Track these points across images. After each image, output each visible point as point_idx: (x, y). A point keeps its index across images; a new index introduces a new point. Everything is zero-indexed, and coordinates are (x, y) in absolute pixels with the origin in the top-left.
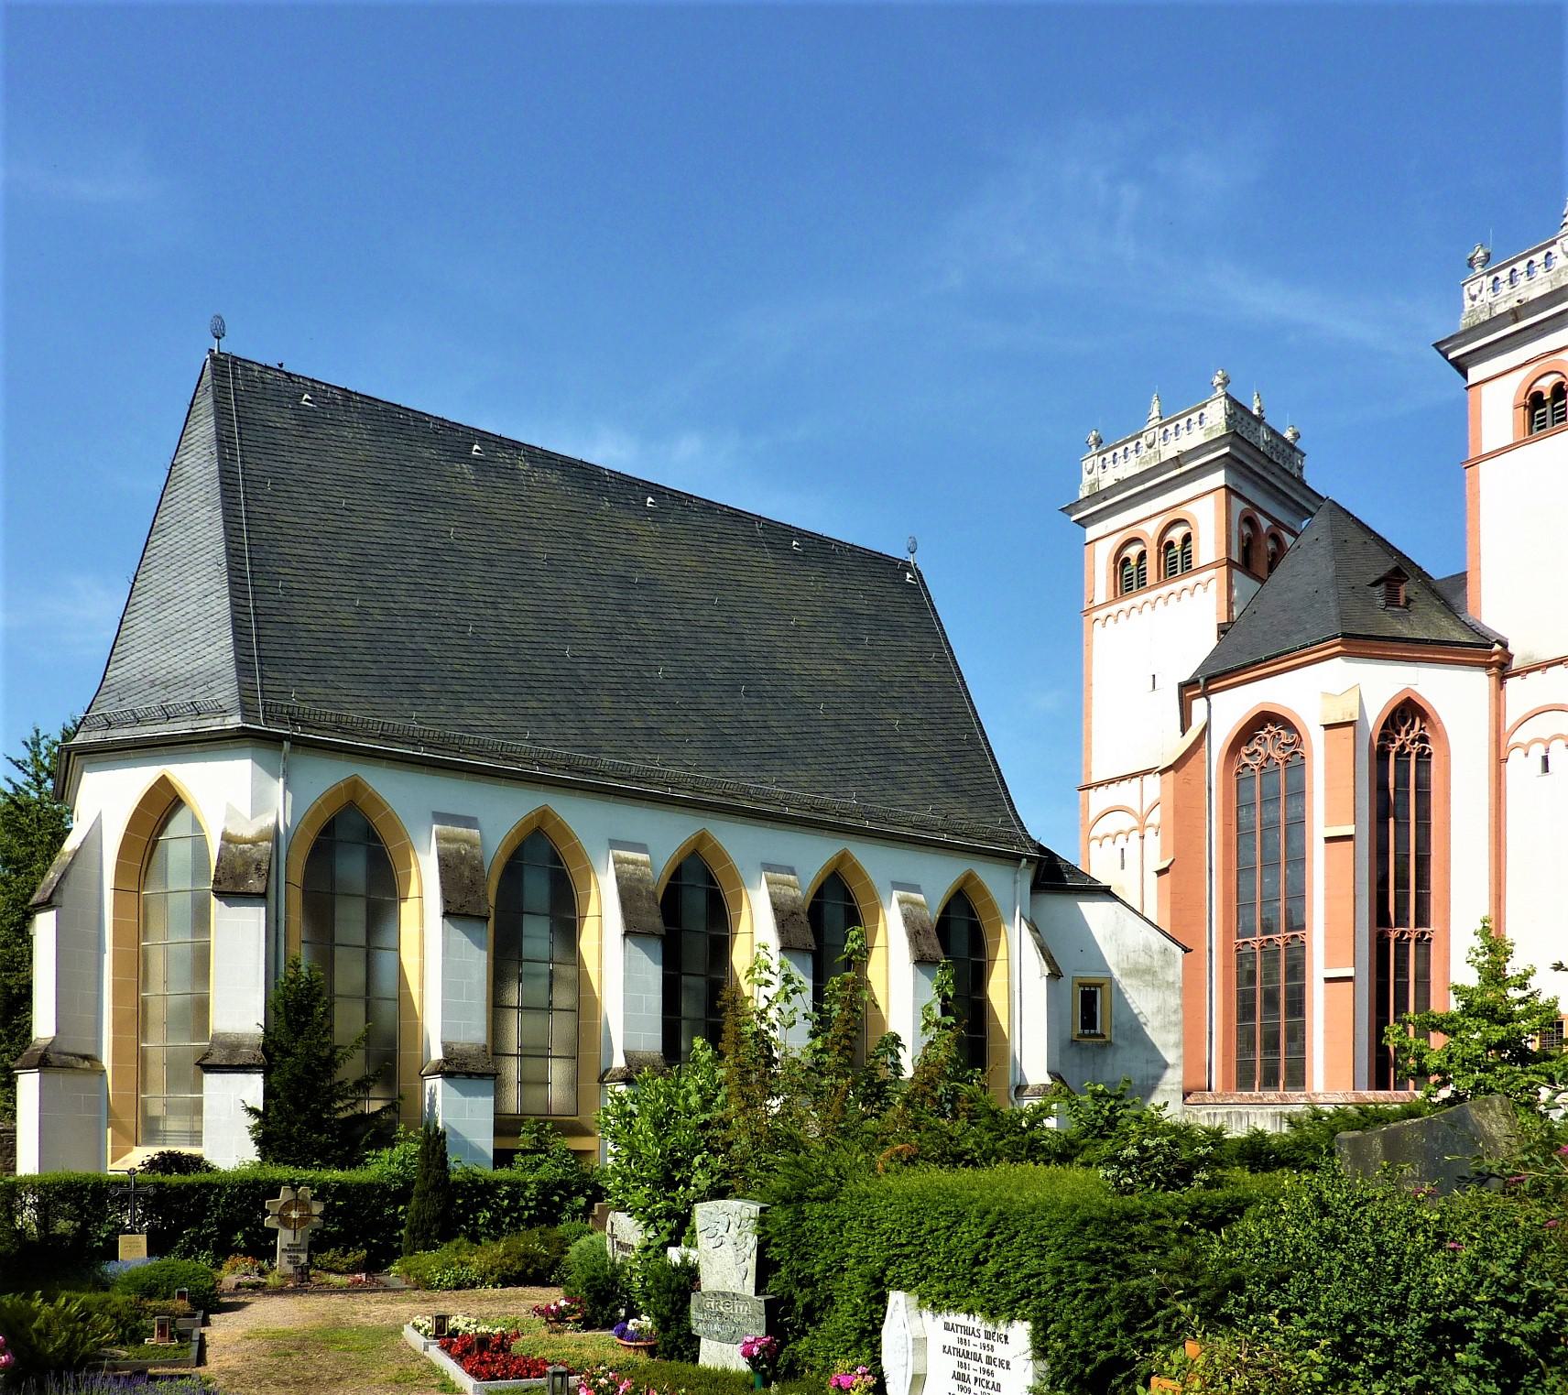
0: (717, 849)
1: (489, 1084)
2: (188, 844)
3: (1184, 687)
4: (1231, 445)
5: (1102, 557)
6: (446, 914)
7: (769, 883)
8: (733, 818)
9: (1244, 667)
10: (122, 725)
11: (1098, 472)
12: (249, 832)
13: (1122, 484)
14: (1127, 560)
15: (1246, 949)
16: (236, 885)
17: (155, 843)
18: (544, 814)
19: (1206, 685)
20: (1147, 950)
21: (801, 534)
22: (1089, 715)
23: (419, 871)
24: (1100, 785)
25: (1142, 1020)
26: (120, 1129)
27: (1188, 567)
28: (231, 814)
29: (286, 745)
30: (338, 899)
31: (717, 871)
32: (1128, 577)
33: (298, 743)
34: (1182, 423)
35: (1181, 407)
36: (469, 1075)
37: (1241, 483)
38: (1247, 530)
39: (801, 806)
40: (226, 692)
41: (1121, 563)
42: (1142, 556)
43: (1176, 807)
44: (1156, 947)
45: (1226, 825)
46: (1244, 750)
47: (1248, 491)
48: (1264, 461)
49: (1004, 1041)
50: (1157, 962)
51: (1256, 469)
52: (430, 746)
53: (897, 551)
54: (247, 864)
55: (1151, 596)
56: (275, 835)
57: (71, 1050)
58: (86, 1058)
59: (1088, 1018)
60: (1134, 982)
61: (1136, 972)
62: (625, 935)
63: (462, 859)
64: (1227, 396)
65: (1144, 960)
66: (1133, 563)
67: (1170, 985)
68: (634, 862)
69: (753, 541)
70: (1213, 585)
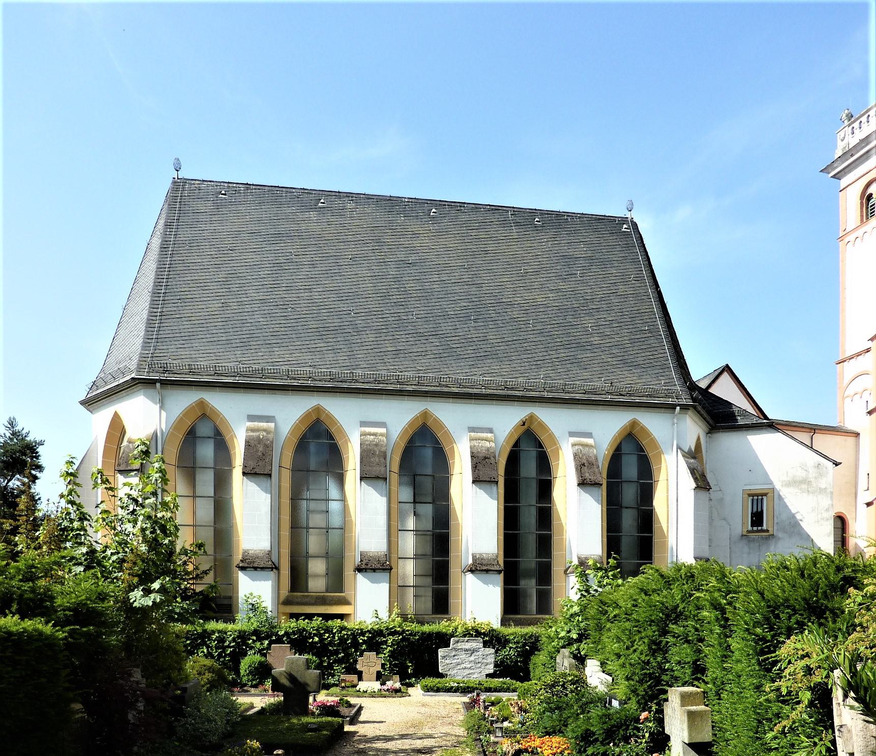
0: (437, 421)
1: (386, 575)
7: (471, 440)
8: (448, 400)
16: (127, 466)
18: (634, 424)
21: (542, 213)
24: (851, 358)
25: (798, 517)
29: (158, 385)
30: (198, 470)
31: (644, 443)
33: (165, 383)
36: (255, 568)
49: (664, 537)
50: (812, 473)
53: (618, 211)
59: (757, 519)
60: (792, 490)
61: (794, 483)
63: (259, 440)
65: (800, 474)
67: (822, 491)
68: (375, 434)
69: (504, 223)
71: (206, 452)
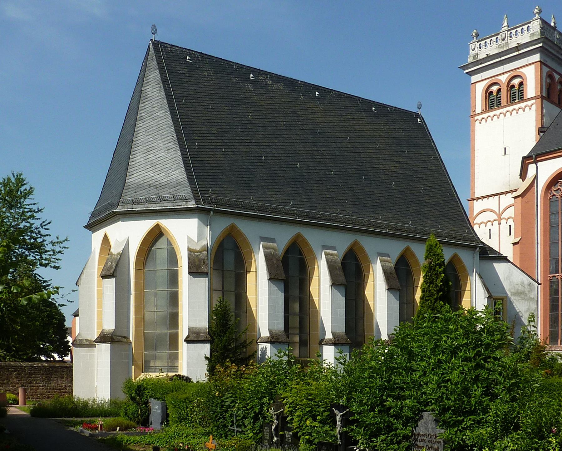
2: (165, 252)
3: (524, 159)
4: (543, 42)
5: (480, 89)
6: (271, 279)
8: (378, 236)
9: (554, 151)
10: (139, 203)
11: (477, 50)
12: (198, 248)
13: (489, 57)
14: (491, 93)
15: (554, 279)
17: (150, 250)
19: (536, 158)
20: (522, 284)
22: (473, 165)
23: (255, 261)
26: (137, 367)
27: (522, 98)
28: (190, 240)
32: (493, 101)
34: (519, 29)
35: (519, 21)
37: (547, 59)
38: (549, 81)
39: (392, 228)
40: (186, 191)
41: (488, 93)
42: (499, 91)
43: (522, 214)
44: (526, 283)
45: (545, 222)
46: (553, 188)
47: (550, 63)
50: (527, 289)
51: (553, 52)
52: (260, 211)
53: (413, 109)
54: (200, 260)
55: (504, 110)
56: (206, 248)
57: (120, 335)
58: (124, 337)
61: (518, 293)
62: (332, 285)
64: (541, 19)
65: (521, 288)
68: (332, 255)
70: (534, 106)
71: (229, 259)
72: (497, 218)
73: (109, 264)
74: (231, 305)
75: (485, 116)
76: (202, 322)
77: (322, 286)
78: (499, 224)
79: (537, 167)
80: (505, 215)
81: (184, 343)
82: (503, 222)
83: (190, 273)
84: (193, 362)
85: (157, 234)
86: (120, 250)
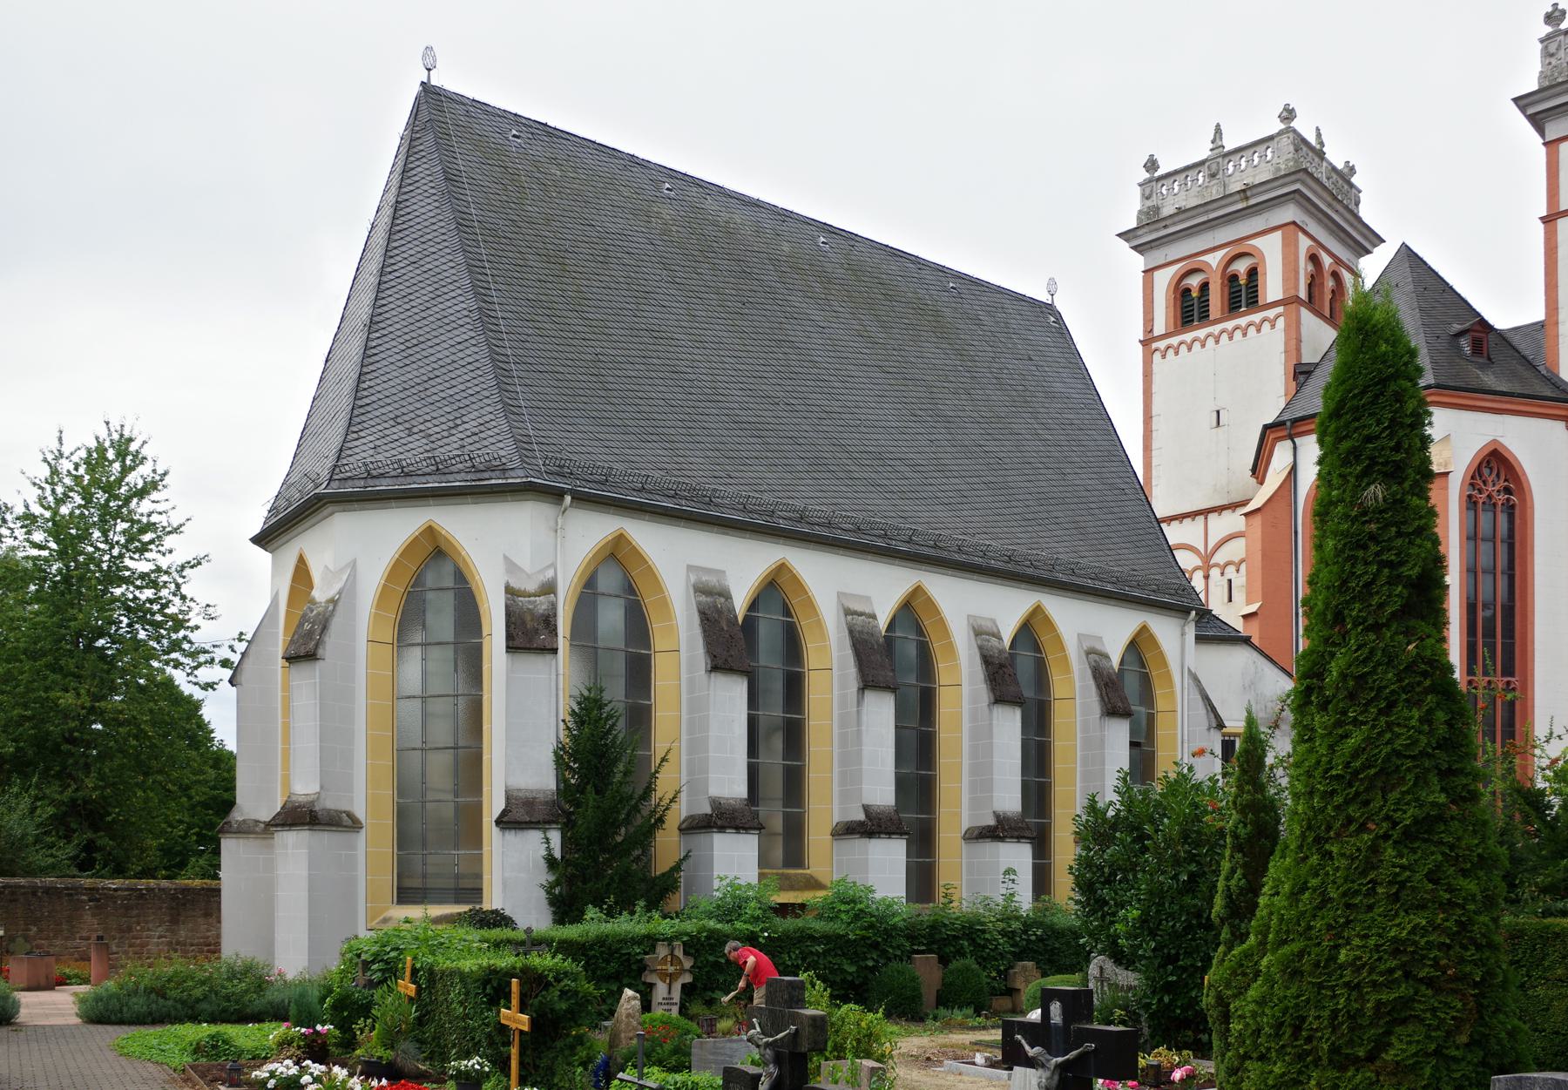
3: (1266, 428)
18: (782, 568)
29: (568, 499)
38: (1310, 267)
42: (1204, 287)
48: (1329, 199)
53: (1043, 297)
66: (1195, 294)
72: (1200, 563)
73: (307, 626)
74: (616, 693)
75: (1174, 341)
76: (541, 777)
77: (1170, 259)
78: (1207, 577)
79: (1295, 448)
80: (1219, 558)
81: (495, 829)
82: (1215, 572)
83: (511, 648)
84: (515, 874)
85: (433, 552)
86: (332, 592)
